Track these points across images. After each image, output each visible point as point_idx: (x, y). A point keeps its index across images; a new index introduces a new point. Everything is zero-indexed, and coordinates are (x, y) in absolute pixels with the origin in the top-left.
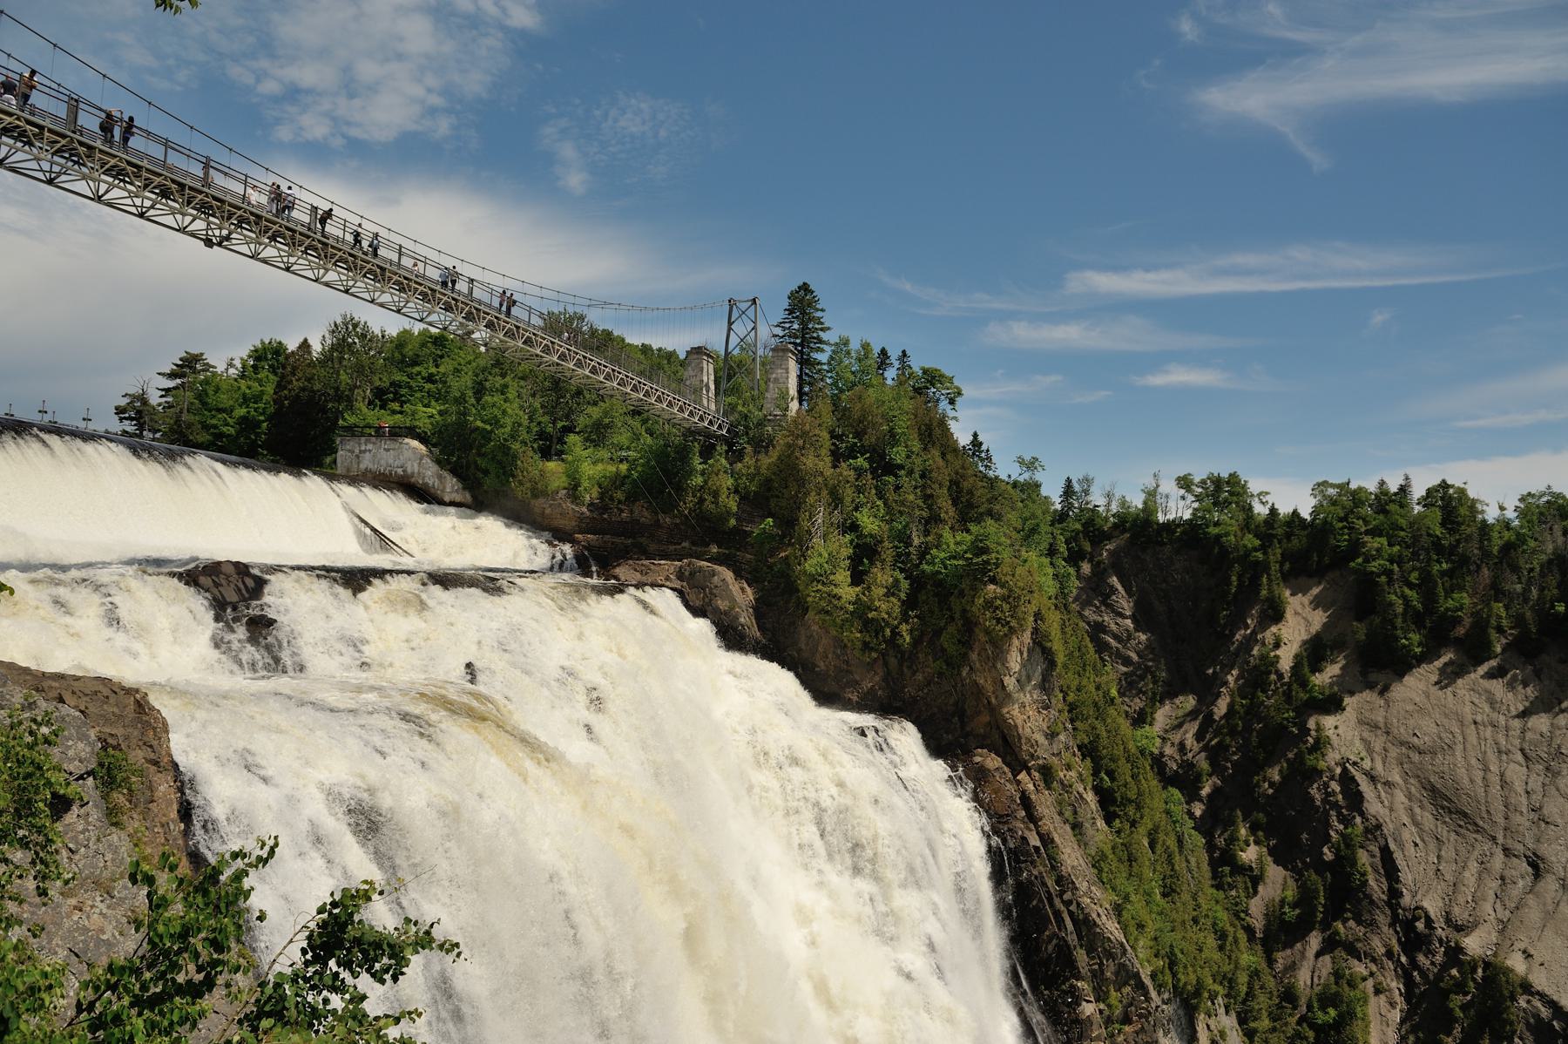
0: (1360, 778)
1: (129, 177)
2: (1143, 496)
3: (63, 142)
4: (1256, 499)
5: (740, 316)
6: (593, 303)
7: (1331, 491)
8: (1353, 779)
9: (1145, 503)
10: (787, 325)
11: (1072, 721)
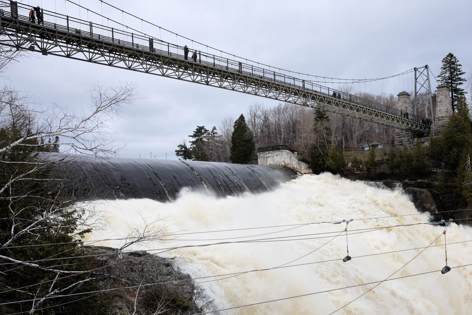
5: (420, 75)
6: (354, 81)
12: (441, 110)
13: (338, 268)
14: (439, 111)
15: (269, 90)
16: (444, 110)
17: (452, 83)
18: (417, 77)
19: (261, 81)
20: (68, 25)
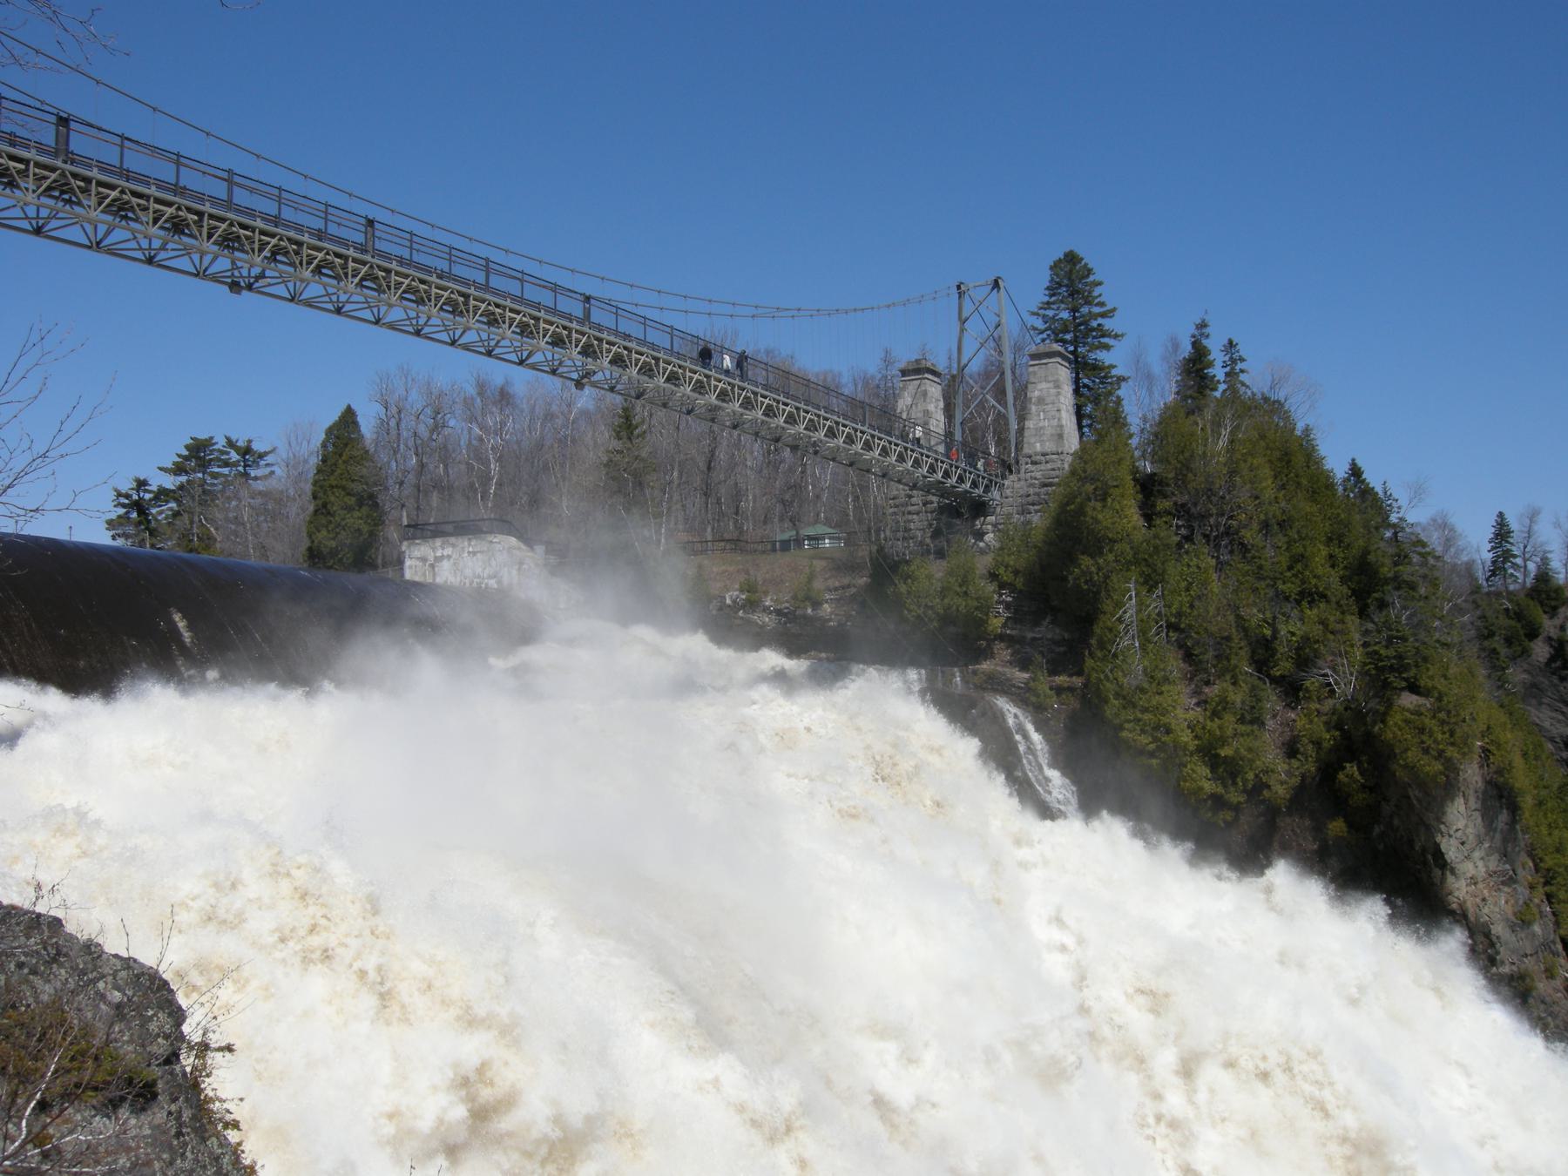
1: (134, 212)
3: (53, 176)
6: (760, 311)
12: (1041, 428)
13: (1441, 747)
16: (1049, 431)
20: (122, 162)
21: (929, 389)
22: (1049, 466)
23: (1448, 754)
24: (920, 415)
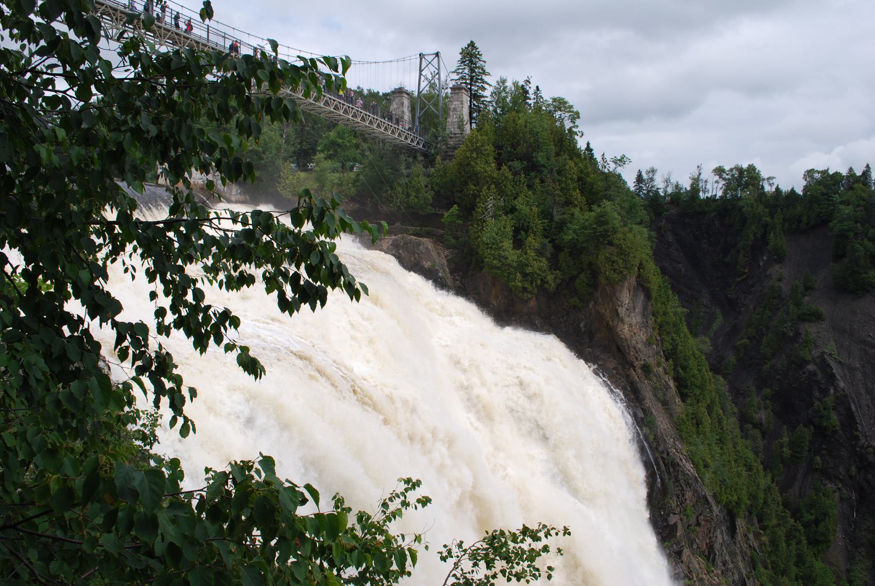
0: (833, 364)
2: (690, 182)
4: (766, 182)
5: (427, 65)
7: (817, 176)
8: (829, 366)
9: (692, 185)
10: (460, 71)
11: (660, 335)
13: (621, 269)
14: (451, 124)
15: (160, 41)
17: (471, 85)
18: (422, 68)
19: (185, 37)
21: (404, 101)
22: (457, 139)
23: (624, 273)
24: (400, 113)
